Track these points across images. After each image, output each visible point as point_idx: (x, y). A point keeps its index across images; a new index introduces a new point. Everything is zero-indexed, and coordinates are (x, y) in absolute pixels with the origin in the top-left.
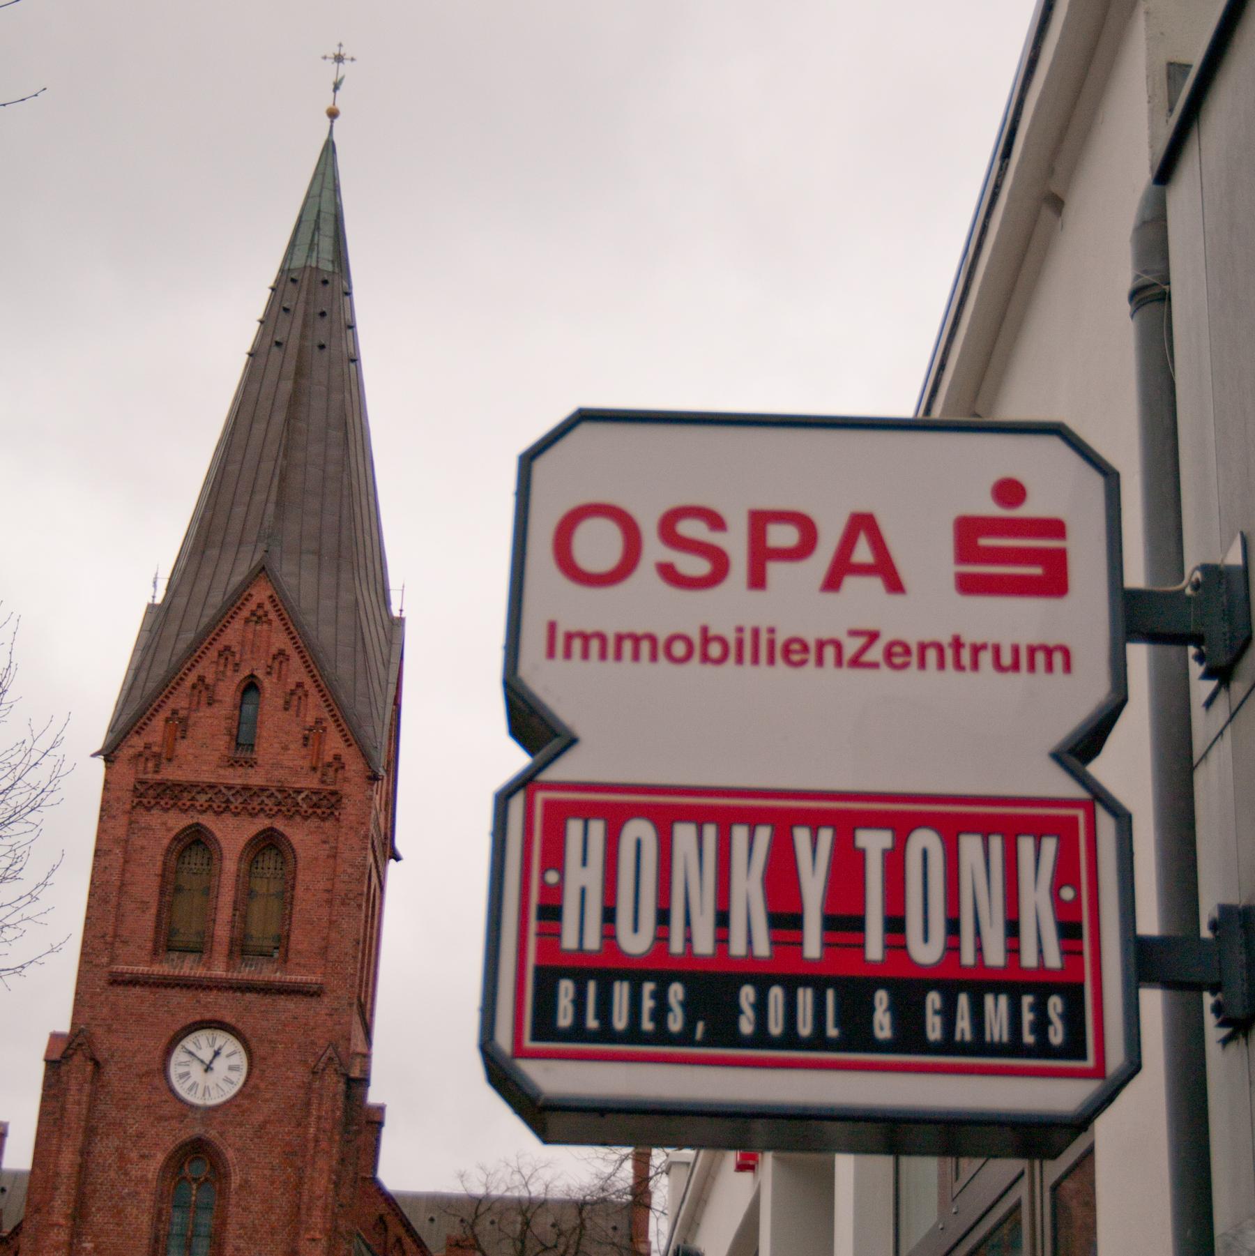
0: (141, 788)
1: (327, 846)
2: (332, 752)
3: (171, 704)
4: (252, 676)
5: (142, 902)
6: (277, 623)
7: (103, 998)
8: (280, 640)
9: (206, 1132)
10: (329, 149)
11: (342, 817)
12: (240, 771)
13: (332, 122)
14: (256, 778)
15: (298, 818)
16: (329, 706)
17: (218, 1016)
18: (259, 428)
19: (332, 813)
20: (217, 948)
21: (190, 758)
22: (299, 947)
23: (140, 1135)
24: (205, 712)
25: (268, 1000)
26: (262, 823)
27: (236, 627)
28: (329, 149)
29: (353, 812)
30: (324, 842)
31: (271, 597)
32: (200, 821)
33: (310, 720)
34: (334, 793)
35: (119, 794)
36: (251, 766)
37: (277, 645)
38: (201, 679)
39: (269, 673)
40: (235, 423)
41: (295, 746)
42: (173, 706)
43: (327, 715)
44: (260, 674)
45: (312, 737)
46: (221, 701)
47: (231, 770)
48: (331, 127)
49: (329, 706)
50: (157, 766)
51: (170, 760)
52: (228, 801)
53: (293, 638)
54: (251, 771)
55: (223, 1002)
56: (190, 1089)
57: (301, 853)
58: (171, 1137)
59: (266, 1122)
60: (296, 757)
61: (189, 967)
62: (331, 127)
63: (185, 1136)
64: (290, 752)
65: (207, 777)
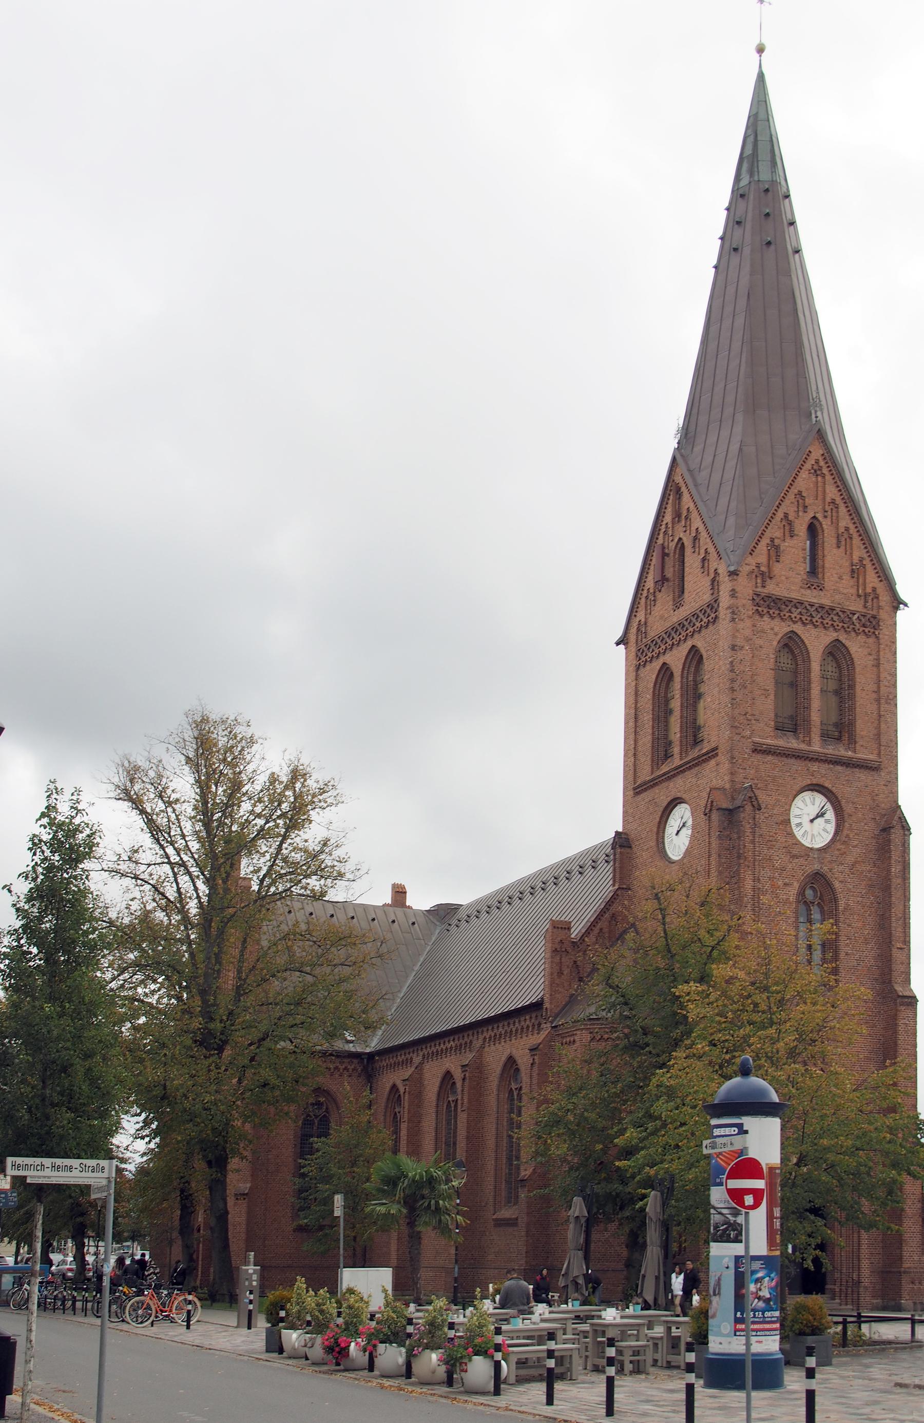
0: (757, 599)
1: (871, 658)
2: (871, 585)
3: (768, 534)
4: (814, 517)
5: (765, 690)
6: (828, 478)
7: (749, 763)
8: (832, 492)
9: (821, 868)
10: (761, 78)
11: (881, 636)
12: (815, 592)
13: (760, 56)
14: (825, 600)
15: (853, 634)
16: (866, 548)
17: (821, 781)
18: (727, 323)
19: (874, 632)
20: (814, 729)
21: (783, 578)
22: (862, 733)
23: (783, 869)
24: (789, 543)
25: (849, 771)
26: (833, 635)
27: (804, 476)
28: (761, 78)
29: (887, 633)
30: (870, 654)
31: (823, 455)
32: (794, 630)
33: (856, 559)
34: (874, 617)
35: (744, 602)
36: (821, 590)
37: (830, 495)
38: (786, 515)
39: (825, 517)
40: (710, 311)
41: (847, 577)
42: (770, 535)
43: (865, 556)
44: (820, 516)
45: (856, 572)
46: (797, 535)
47: (809, 591)
48: (760, 60)
49: (866, 548)
50: (764, 581)
51: (771, 578)
52: (811, 616)
53: (840, 491)
54: (822, 593)
55: (823, 772)
56: (803, 835)
57: (857, 662)
58: (802, 869)
59: (856, 862)
60: (847, 586)
61: (793, 743)
62: (760, 60)
63: (809, 870)
64: (844, 581)
65: (794, 595)
